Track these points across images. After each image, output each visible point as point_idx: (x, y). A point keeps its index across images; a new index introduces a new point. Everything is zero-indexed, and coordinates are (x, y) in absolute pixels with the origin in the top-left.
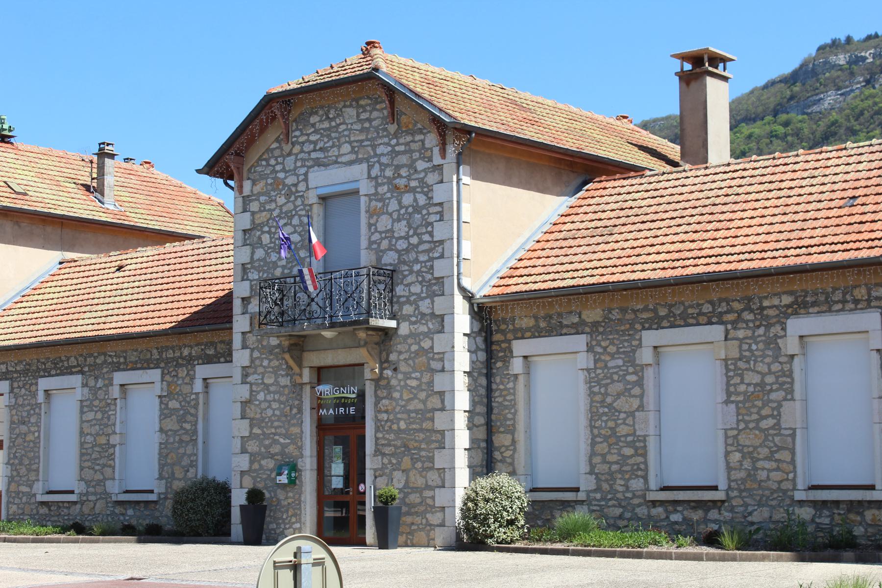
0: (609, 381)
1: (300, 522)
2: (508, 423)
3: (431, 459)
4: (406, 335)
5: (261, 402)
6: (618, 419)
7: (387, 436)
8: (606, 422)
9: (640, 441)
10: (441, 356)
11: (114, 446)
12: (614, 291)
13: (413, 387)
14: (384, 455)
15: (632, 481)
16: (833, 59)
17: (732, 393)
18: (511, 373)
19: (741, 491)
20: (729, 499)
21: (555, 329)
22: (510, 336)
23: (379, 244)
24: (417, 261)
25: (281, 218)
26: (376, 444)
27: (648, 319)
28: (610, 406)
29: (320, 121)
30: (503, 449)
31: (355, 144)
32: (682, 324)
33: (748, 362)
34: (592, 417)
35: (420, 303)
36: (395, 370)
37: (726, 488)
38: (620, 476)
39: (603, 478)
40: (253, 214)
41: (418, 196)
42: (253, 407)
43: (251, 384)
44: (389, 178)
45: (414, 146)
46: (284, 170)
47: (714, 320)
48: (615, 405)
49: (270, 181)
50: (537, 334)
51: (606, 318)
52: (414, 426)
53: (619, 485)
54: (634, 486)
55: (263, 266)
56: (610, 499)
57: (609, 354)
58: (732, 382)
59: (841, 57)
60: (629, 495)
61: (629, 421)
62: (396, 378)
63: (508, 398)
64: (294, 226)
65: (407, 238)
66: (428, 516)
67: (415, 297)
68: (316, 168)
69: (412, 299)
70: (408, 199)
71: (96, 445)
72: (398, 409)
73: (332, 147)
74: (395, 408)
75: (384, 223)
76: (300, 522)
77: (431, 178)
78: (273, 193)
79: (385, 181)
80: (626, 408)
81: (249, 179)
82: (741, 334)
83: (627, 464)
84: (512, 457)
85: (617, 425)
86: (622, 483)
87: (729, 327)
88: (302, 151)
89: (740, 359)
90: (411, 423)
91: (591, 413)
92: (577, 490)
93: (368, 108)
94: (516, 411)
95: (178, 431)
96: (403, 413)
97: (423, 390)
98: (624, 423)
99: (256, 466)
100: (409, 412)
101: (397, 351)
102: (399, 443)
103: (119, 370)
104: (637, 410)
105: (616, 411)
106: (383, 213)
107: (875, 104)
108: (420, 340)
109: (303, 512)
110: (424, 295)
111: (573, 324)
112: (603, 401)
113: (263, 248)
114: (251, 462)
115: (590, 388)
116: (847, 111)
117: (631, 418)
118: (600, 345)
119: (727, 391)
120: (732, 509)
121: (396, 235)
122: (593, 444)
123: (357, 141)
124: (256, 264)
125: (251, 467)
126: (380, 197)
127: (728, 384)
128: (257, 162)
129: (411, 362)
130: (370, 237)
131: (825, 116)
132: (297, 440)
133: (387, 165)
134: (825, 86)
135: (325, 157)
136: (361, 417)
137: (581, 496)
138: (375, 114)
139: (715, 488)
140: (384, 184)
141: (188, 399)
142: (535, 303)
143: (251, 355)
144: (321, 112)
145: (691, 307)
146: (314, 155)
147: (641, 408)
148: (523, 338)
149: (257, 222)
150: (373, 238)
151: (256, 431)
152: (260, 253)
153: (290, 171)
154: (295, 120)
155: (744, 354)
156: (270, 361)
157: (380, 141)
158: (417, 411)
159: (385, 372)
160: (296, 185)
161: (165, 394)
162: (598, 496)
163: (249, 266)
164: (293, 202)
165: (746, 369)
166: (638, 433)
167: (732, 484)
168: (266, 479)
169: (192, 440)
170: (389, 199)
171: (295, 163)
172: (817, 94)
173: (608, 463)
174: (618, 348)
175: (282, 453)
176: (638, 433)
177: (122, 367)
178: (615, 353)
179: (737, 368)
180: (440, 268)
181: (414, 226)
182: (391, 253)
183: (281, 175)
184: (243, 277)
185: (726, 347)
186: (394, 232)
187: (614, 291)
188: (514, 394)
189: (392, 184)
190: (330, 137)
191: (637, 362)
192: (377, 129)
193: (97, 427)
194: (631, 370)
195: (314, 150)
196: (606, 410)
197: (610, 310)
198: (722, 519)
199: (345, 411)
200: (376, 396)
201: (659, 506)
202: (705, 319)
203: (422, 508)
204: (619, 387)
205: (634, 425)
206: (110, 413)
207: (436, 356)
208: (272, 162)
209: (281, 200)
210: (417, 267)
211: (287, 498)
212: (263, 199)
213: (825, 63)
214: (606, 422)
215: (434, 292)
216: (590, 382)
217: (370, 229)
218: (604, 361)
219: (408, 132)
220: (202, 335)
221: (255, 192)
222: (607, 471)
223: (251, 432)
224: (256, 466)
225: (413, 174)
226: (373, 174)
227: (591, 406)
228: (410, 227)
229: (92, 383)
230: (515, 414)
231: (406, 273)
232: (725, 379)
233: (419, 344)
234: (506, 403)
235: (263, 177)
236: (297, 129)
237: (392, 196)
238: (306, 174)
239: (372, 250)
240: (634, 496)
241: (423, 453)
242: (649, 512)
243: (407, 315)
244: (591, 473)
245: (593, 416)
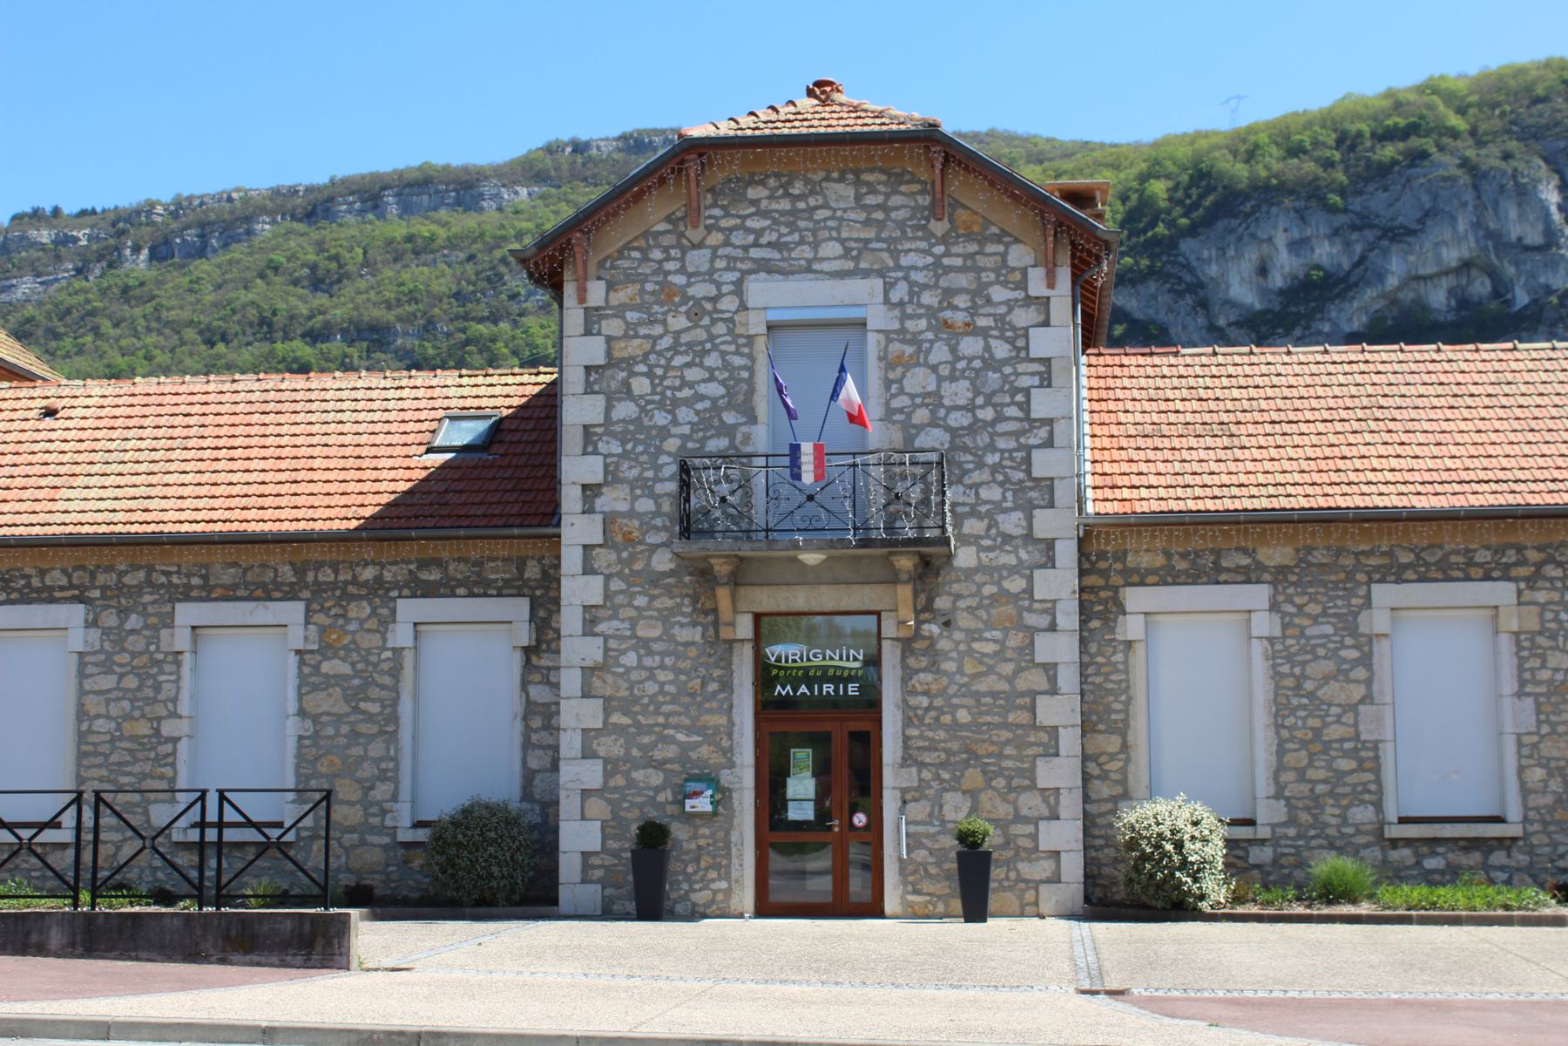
0: (1309, 657)
1: (728, 878)
2: (1114, 717)
3: (1031, 774)
4: (968, 569)
5: (629, 670)
6: (1328, 715)
7: (930, 734)
8: (1304, 719)
9: (1367, 749)
11: (175, 740)
12: (1300, 521)
13: (986, 655)
14: (922, 765)
15: (1354, 810)
16: (33, 233)
18: (1120, 638)
19: (1545, 823)
20: (1527, 836)
22: (1116, 580)
23: (909, 415)
24: (992, 448)
25: (677, 353)
26: (906, 746)
27: (1380, 566)
28: (1311, 695)
29: (771, 197)
30: (1103, 759)
31: (853, 244)
33: (1553, 637)
34: (1277, 711)
35: (1000, 518)
36: (947, 624)
38: (1331, 801)
39: (1301, 805)
41: (993, 342)
43: (606, 638)
44: (929, 308)
46: (682, 270)
47: (1495, 574)
48: (1320, 693)
49: (649, 287)
51: (1300, 560)
52: (989, 719)
56: (1313, 837)
57: (1309, 616)
58: (1527, 666)
59: (45, 233)
60: (1349, 830)
61: (1349, 718)
62: (950, 637)
63: (1114, 677)
65: (970, 408)
66: (1020, 866)
67: (988, 507)
68: (763, 275)
69: (983, 509)
71: (121, 738)
72: (952, 689)
75: (920, 380)
76: (728, 878)
77: (1022, 317)
78: (656, 308)
79: (922, 311)
80: (1342, 699)
81: (599, 278)
82: (1541, 596)
83: (1345, 784)
84: (1124, 771)
85: (1325, 725)
86: (1337, 812)
87: (1522, 585)
88: (727, 243)
89: (1540, 633)
90: (981, 714)
93: (882, 188)
94: (1130, 699)
95: (347, 715)
96: (963, 696)
98: (1338, 721)
99: (619, 781)
100: (977, 696)
101: (949, 594)
102: (955, 746)
103: (187, 598)
104: (1362, 701)
105: (1323, 703)
106: (918, 364)
107: (88, 301)
108: (1001, 578)
109: (735, 861)
110: (1009, 504)
111: (1239, 567)
112: (1298, 686)
113: (635, 401)
114: (607, 775)
115: (1274, 666)
116: (49, 307)
117: (1351, 715)
118: (1292, 602)
119: (1520, 677)
121: (946, 402)
122: (1281, 752)
123: (856, 240)
124: (618, 428)
125: (605, 783)
126: (908, 336)
127: (1520, 668)
128: (620, 252)
130: (887, 403)
131: (16, 310)
132: (722, 739)
133: (925, 287)
134: (19, 268)
135: (783, 260)
136: (871, 704)
137: (1263, 832)
138: (896, 200)
140: (920, 317)
141: (374, 659)
142: (1196, 531)
143: (606, 587)
144: (772, 182)
145: (1457, 553)
146: (755, 253)
148: (1142, 584)
150: (896, 403)
151: (616, 718)
152: (626, 410)
154: (711, 190)
155: (1548, 625)
156: (653, 598)
157: (908, 246)
158: (995, 695)
159: (925, 627)
160: (714, 300)
161: (316, 647)
162: (1292, 832)
165: (1551, 648)
166: (1363, 737)
168: (643, 805)
169: (382, 732)
170: (932, 342)
171: (712, 261)
172: (7, 279)
173: (1310, 781)
174: (1325, 608)
175: (683, 758)
176: (1363, 737)
177: (194, 594)
179: (1534, 646)
180: (1043, 463)
181: (987, 390)
182: (936, 431)
183: (679, 280)
184: (585, 448)
185: (1520, 617)
187: (1300, 521)
188: (1127, 672)
190: (793, 228)
192: (901, 224)
194: (1349, 641)
195: (756, 245)
196: (1305, 701)
197: (1309, 550)
198: (1513, 864)
199: (836, 690)
202: (1481, 572)
203: (1009, 854)
204: (1328, 666)
205: (1356, 725)
206: (161, 678)
207: (1036, 606)
209: (679, 322)
210: (992, 459)
211: (695, 837)
212: (632, 316)
213: (22, 238)
214: (1304, 719)
216: (1274, 658)
217: (888, 388)
219: (969, 237)
220: (407, 546)
223: (605, 722)
224: (619, 781)
225: (982, 306)
227: (1276, 695)
228: (977, 393)
229: (110, 619)
230: (1128, 703)
231: (971, 466)
232: (1516, 661)
233: (999, 584)
234: (1111, 686)
235: (630, 278)
236: (714, 205)
237: (937, 339)
238: (739, 284)
239: (894, 423)
240: (1358, 832)
241: (1009, 764)
243: (971, 535)
244: (1278, 796)
245: (1280, 709)
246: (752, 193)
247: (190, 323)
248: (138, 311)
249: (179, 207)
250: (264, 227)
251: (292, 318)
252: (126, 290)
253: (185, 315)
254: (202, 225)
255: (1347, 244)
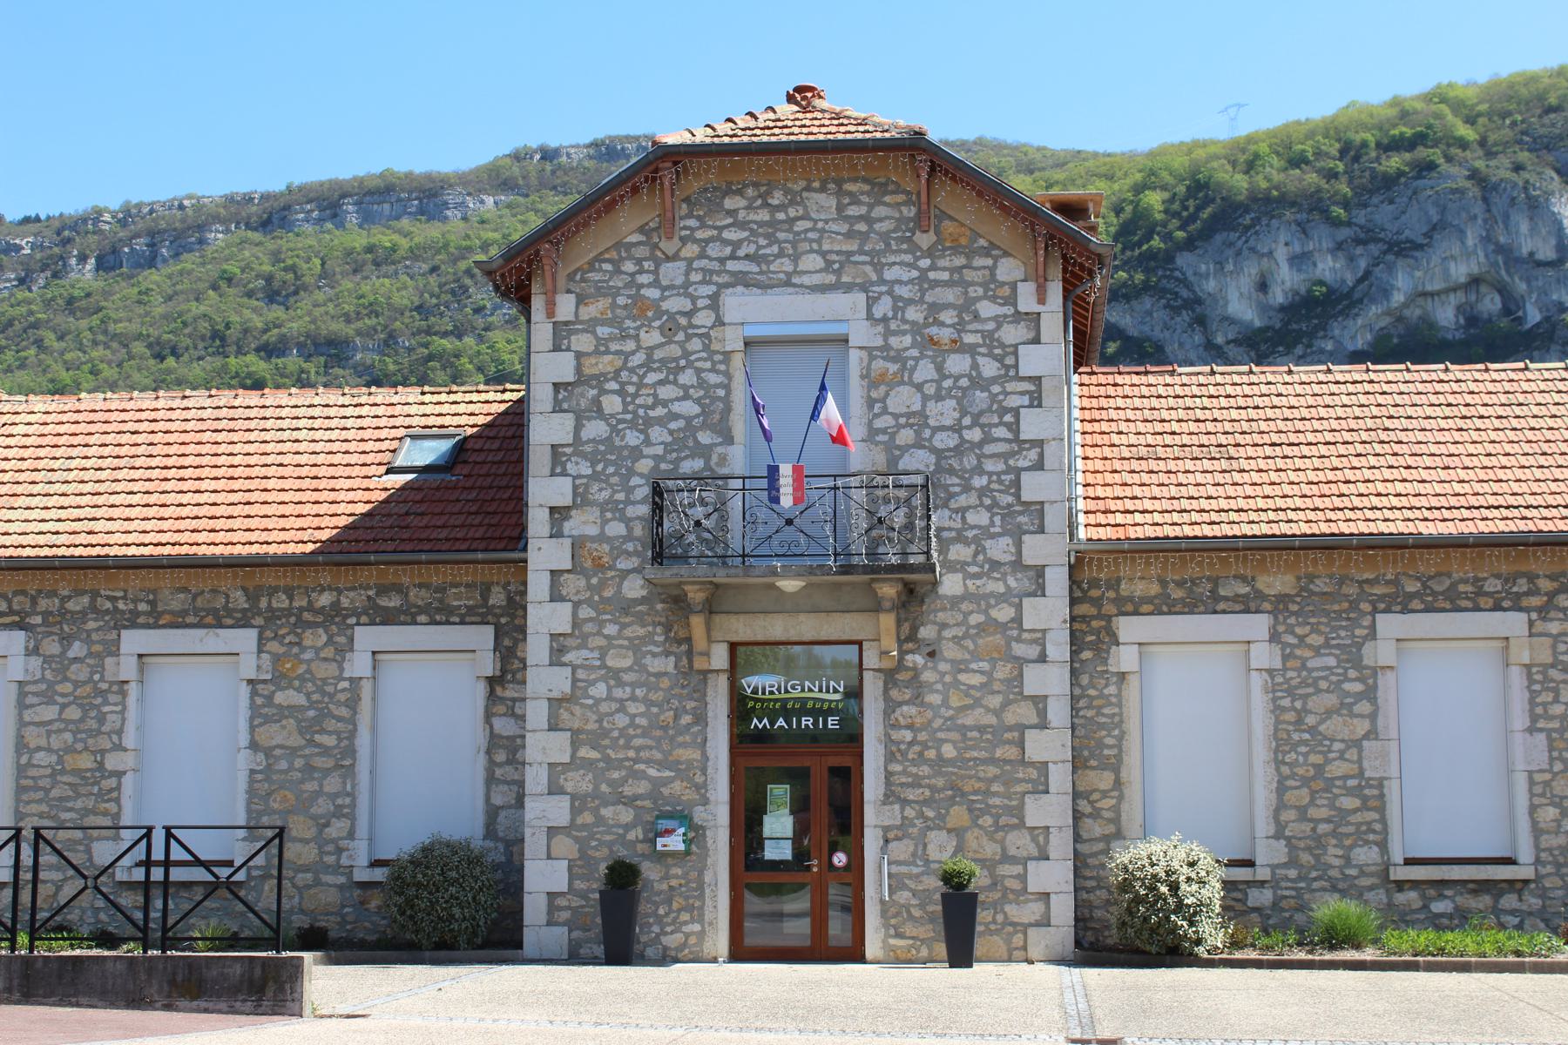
0: (1311, 690)
1: (701, 920)
3: (1019, 812)
5: (598, 701)
6: (1330, 751)
7: (914, 770)
9: (1371, 787)
10: (1039, 635)
11: (120, 774)
14: (905, 802)
15: (1358, 850)
17: (1540, 716)
20: (1539, 878)
21: (1202, 601)
26: (888, 783)
27: (1385, 595)
28: (1312, 730)
29: (748, 208)
30: (1095, 796)
31: (834, 257)
32: (1448, 606)
35: (988, 544)
37: (1532, 860)
38: (1334, 842)
40: (579, 356)
41: (980, 360)
42: (577, 710)
43: (574, 668)
44: (914, 323)
45: (969, 275)
46: (656, 284)
47: (1506, 604)
48: (1322, 728)
49: (621, 301)
50: (1165, 609)
51: (1302, 589)
52: (975, 754)
53: (1333, 855)
54: (1362, 857)
55: (604, 454)
56: (1315, 879)
57: (1310, 647)
58: (1538, 700)
60: (1353, 872)
61: (1352, 754)
62: (935, 668)
63: (1106, 711)
64: (685, 388)
65: (957, 428)
66: (1007, 908)
67: (975, 532)
68: (740, 289)
69: (970, 534)
70: (958, 364)
71: (63, 772)
73: (777, 256)
74: (930, 722)
75: (903, 399)
76: (701, 920)
79: (907, 327)
81: (569, 291)
82: (1554, 627)
83: (1348, 823)
84: (1116, 809)
85: (1328, 761)
86: (1340, 853)
87: (1534, 616)
88: (702, 255)
89: (1553, 666)
91: (1276, 738)
92: (1249, 864)
94: (1123, 733)
95: (301, 748)
97: (993, 693)
98: (1341, 758)
99: (587, 818)
100: (963, 729)
103: (134, 625)
104: (1366, 736)
105: (1325, 738)
106: (902, 383)
107: (31, 313)
108: (989, 606)
109: (708, 902)
110: (997, 530)
111: (1237, 596)
112: (1299, 721)
113: (606, 420)
114: (575, 812)
115: (1274, 700)
117: (1355, 751)
118: (1293, 633)
120: (1543, 894)
121: (932, 422)
122: (1281, 789)
123: (838, 253)
125: (573, 820)
126: (892, 353)
127: (1532, 702)
128: (591, 264)
129: (969, 644)
133: (910, 302)
138: (880, 211)
139: (1509, 861)
140: (904, 333)
141: (330, 689)
143: (575, 614)
144: (750, 192)
145: (1466, 581)
147: (1372, 734)
148: (1136, 613)
149: (587, 371)
150: (878, 424)
151: (585, 752)
152: (595, 429)
153: (672, 287)
154: (687, 200)
156: (623, 626)
157: (892, 259)
158: (981, 729)
159: (909, 657)
160: (689, 315)
162: (1293, 873)
163: (568, 450)
164: (681, 344)
167: (1543, 855)
169: (338, 767)
171: (687, 274)
173: (1311, 820)
174: (1327, 639)
175: (654, 795)
176: (1367, 774)
178: (1320, 647)
179: (1547, 679)
182: (921, 452)
183: (653, 293)
184: (553, 469)
185: (1531, 648)
186: (927, 417)
188: (1120, 705)
189: (922, 335)
190: (772, 239)
191: (1366, 662)
193: (68, 736)
194: (1352, 674)
195: (733, 257)
196: (1307, 736)
197: (1311, 578)
198: (1524, 908)
199: (816, 723)
200: (887, 697)
201: (1410, 889)
202: (1491, 602)
204: (1331, 700)
205: (1360, 761)
208: (629, 267)
210: (979, 482)
211: (666, 877)
212: (603, 331)
215: (1019, 526)
216: (1274, 691)
218: (1300, 658)
219: (956, 249)
221: (584, 316)
222: (1309, 833)
223: (573, 756)
224: (587, 818)
225: (970, 322)
226: (878, 313)
227: (1276, 730)
228: (964, 413)
229: (52, 647)
230: (1121, 738)
231: (957, 489)
233: (986, 612)
235: (601, 291)
236: (690, 216)
237: (923, 356)
238: (715, 299)
239: (877, 444)
240: (1362, 873)
241: (997, 801)
242: (1390, 899)
244: (1277, 836)
245: (1281, 745)
246: (729, 203)
247: (139, 337)
248: (84, 324)
249: (127, 216)
250: (217, 236)
251: (246, 331)
252: (71, 301)
253: (134, 327)
254: (152, 233)
255: (1352, 259)
